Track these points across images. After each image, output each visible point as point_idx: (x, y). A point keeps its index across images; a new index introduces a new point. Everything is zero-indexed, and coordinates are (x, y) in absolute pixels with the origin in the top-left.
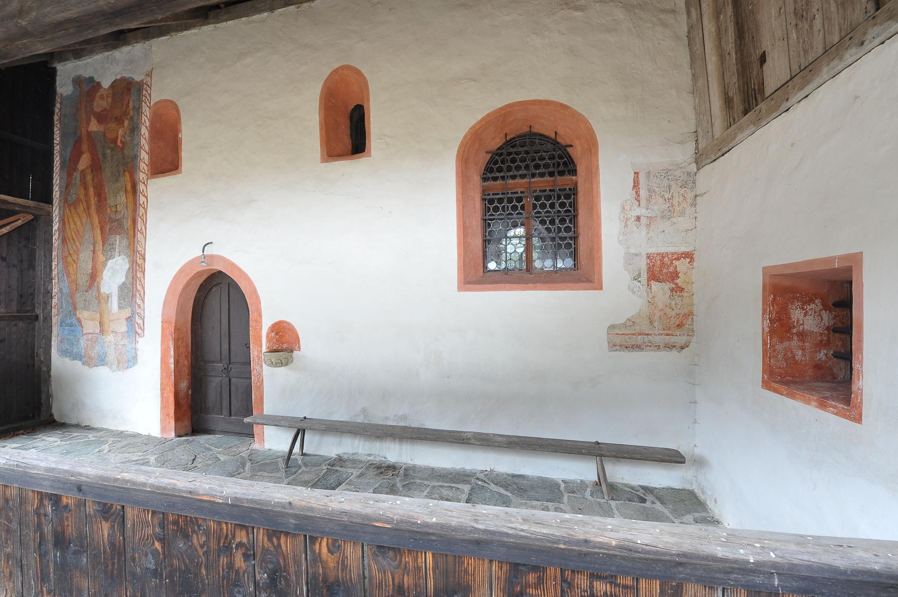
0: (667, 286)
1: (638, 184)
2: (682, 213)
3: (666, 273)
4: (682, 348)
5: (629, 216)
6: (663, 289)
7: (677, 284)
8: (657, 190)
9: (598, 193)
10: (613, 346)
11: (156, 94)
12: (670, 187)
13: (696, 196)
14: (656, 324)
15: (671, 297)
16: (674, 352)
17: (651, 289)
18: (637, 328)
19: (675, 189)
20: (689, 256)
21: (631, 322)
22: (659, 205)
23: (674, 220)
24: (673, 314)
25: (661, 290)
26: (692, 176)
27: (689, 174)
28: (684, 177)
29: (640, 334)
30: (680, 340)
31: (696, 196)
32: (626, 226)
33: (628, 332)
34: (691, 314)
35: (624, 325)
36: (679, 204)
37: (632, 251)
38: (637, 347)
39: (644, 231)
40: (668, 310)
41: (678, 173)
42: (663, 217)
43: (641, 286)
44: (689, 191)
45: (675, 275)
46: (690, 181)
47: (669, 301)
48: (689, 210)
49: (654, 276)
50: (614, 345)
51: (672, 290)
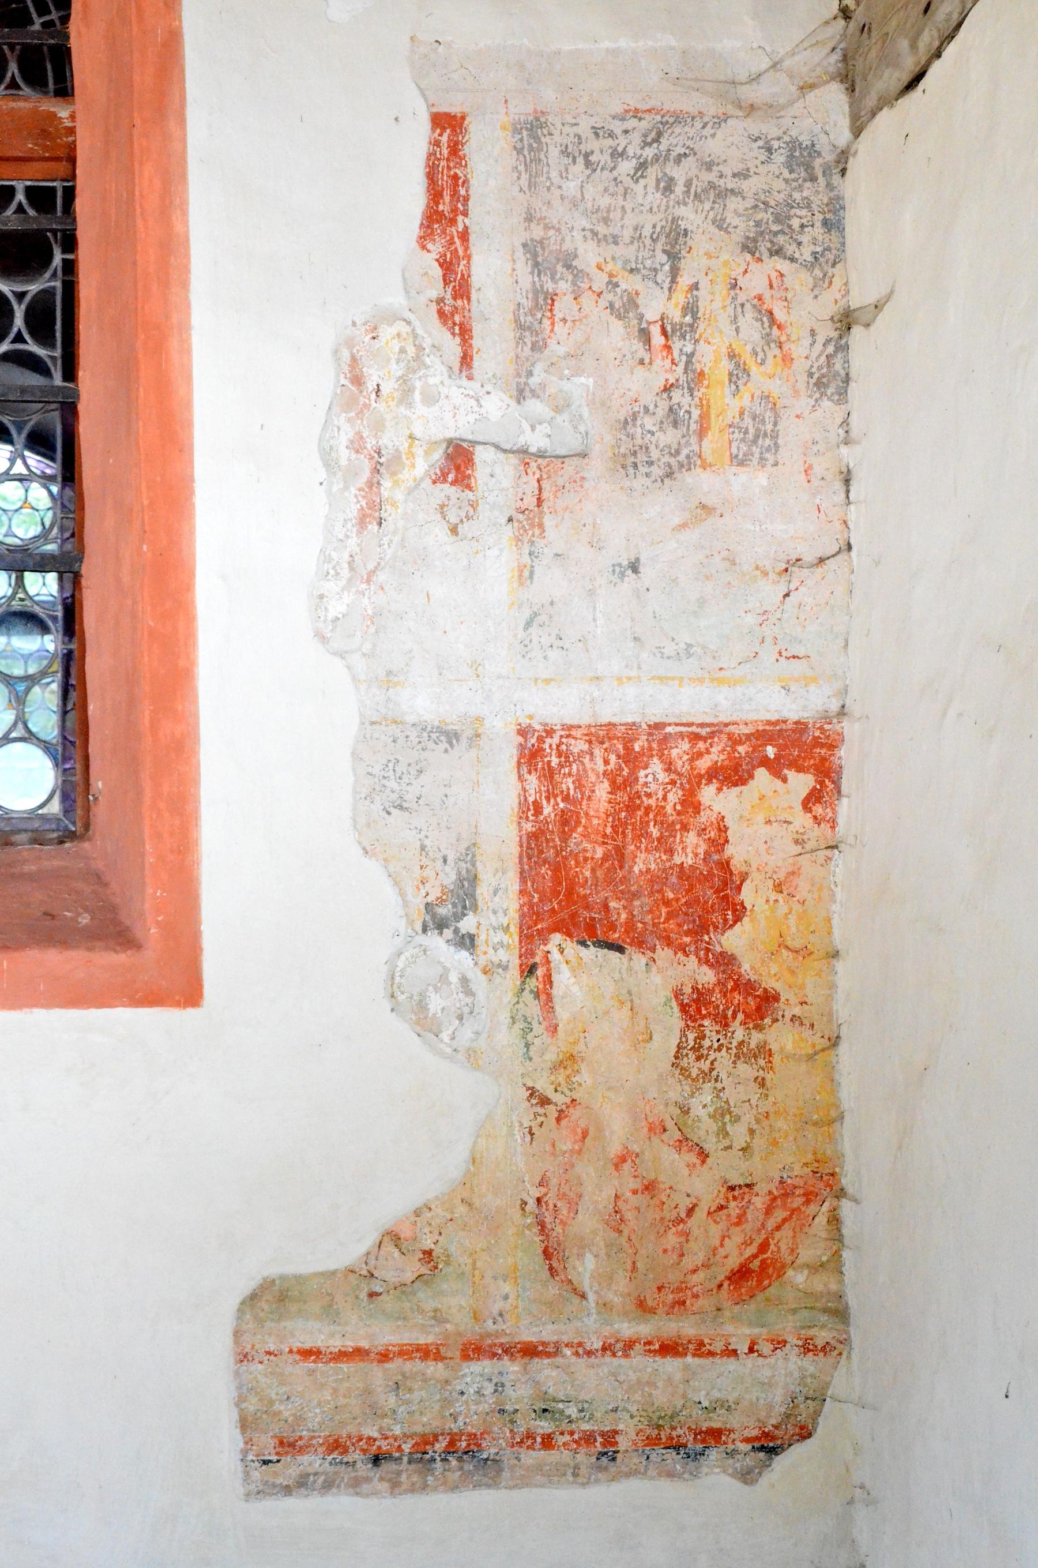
0: (658, 978)
1: (461, 203)
2: (758, 441)
3: (656, 881)
4: (768, 1447)
5: (391, 440)
6: (629, 1001)
7: (724, 962)
8: (589, 255)
9: (172, 249)
10: (281, 1454)
11: (798, 1251)
12: (674, 242)
13: (846, 321)
14: (585, 1268)
15: (689, 1054)
16: (716, 1481)
17: (545, 995)
18: (455, 1306)
19: (710, 257)
20: (806, 751)
21: (414, 1255)
22: (601, 375)
23: (703, 483)
24: (703, 1186)
25: (616, 1000)
26: (818, 167)
27: (801, 158)
28: (770, 179)
29: (473, 1351)
30: (750, 1386)
31: (846, 321)
32: (372, 514)
33: (387, 1334)
34: (821, 1185)
35: (364, 1282)
36: (739, 374)
37: (421, 703)
38: (454, 1453)
39: (499, 557)
40: (669, 1162)
41: (730, 144)
42: (629, 461)
43: (476, 975)
44: (798, 280)
45: (712, 896)
46: (803, 214)
47: (677, 1090)
48: (805, 421)
49: (568, 901)
50: (288, 1446)
51: (694, 1006)
